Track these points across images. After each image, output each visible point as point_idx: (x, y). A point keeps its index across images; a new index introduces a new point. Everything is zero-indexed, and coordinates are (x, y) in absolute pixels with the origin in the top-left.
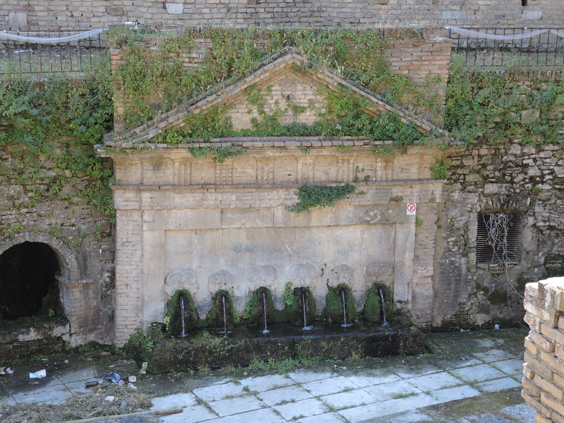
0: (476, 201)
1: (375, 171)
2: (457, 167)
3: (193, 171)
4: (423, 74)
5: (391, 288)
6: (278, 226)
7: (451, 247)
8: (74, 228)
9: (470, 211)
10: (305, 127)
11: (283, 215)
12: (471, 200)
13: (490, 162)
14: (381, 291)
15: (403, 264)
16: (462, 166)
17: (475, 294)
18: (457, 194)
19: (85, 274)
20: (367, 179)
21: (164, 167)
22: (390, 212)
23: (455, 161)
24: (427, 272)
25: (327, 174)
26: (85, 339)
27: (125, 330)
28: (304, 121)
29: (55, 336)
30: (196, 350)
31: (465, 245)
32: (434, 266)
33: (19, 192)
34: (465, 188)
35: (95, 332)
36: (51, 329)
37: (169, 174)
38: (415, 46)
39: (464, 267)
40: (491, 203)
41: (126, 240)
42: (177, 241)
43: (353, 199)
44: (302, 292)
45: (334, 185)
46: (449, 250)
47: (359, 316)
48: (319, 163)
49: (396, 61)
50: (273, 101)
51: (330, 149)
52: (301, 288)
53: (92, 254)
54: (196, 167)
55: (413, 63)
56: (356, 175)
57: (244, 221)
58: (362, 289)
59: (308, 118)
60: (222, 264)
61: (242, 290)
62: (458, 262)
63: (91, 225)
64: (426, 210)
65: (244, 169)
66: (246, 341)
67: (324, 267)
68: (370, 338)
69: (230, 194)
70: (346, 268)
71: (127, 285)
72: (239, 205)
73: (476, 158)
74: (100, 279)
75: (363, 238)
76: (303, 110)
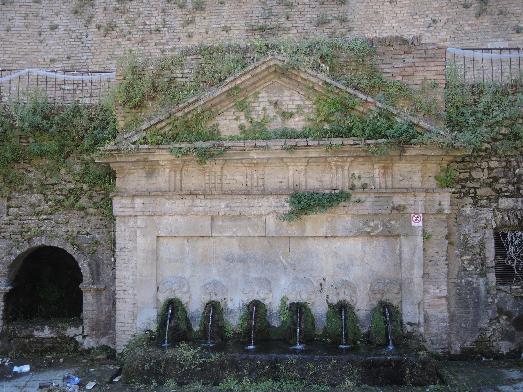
0: (490, 216)
1: (373, 178)
2: (466, 180)
3: (184, 177)
4: (418, 80)
5: (400, 308)
6: (269, 236)
7: (466, 266)
8: (89, 237)
9: (485, 228)
10: (293, 131)
11: (275, 224)
12: (485, 215)
13: (502, 175)
14: (387, 311)
15: (411, 281)
16: (472, 179)
17: (497, 319)
18: (469, 209)
19: (98, 280)
20: (364, 187)
21: (156, 175)
22: (393, 222)
23: (463, 174)
24: (440, 292)
25: (321, 181)
26: (98, 342)
27: (124, 336)
28: (293, 127)
29: (68, 336)
30: (167, 361)
31: (483, 265)
32: (448, 286)
33: (40, 201)
34: (477, 202)
35: (107, 337)
36: (64, 329)
37: (163, 180)
38: (406, 53)
39: (483, 288)
40: (507, 219)
41: (123, 246)
42: (170, 249)
43: (350, 208)
44: (297, 308)
45: (327, 192)
46: (465, 269)
47: (363, 338)
48: (312, 170)
49: (387, 68)
50: (260, 108)
51: (318, 149)
52: (298, 303)
53: (105, 262)
54: (186, 174)
55: (406, 69)
56: (353, 183)
57: (235, 230)
58: (366, 308)
59: (297, 123)
60: (215, 274)
61: (235, 302)
62: (476, 283)
63: (105, 235)
64: (434, 223)
65: (236, 176)
66: (221, 356)
67: (323, 282)
68: (368, 362)
69: (219, 201)
70: (347, 284)
71: (125, 291)
72: (228, 212)
73: (486, 170)
74: (112, 286)
75: (364, 251)
76: (291, 115)
